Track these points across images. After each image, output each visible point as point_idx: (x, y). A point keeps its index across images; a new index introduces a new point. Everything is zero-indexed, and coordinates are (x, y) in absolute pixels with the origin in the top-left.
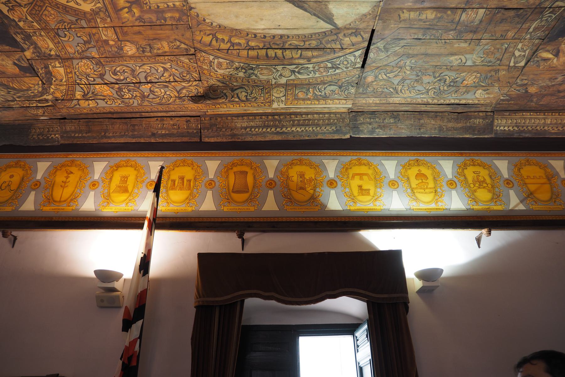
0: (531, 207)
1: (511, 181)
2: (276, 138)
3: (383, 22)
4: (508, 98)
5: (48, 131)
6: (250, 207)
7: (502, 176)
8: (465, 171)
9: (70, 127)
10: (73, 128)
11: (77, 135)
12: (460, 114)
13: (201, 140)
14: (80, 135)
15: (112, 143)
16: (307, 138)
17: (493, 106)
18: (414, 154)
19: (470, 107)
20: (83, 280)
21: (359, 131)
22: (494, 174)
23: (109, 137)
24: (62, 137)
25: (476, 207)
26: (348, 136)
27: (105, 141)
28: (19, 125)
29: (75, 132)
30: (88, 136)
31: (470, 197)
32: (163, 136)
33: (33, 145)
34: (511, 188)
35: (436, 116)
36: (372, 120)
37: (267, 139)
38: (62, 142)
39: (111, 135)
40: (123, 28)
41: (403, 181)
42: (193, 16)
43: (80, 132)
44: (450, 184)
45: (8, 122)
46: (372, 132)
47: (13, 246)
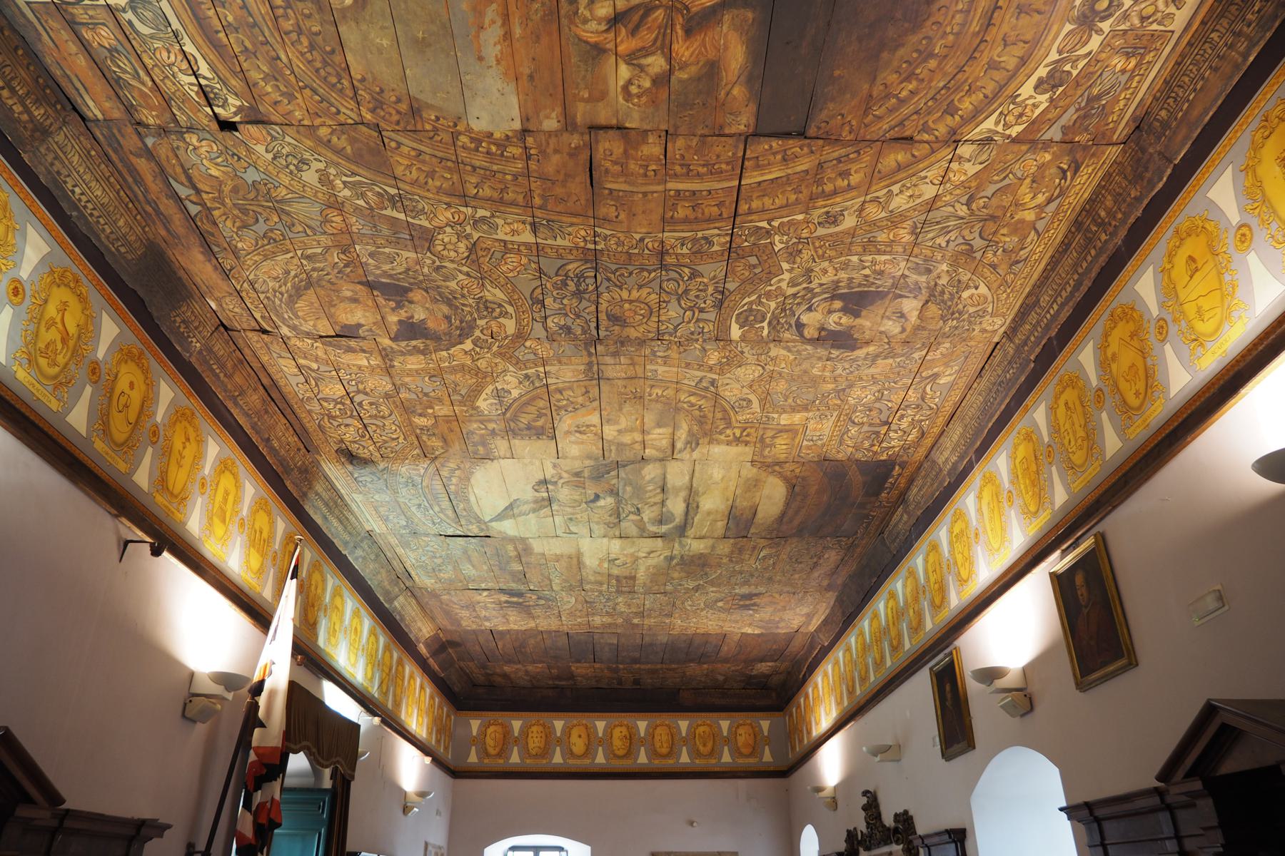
0: (15, 368)
1: (24, 290)
5: (196, 328)
6: (53, 400)
7: (17, 265)
8: (55, 289)
9: (220, 348)
10: (221, 353)
11: (215, 367)
14: (218, 371)
15: (232, 414)
16: (330, 536)
18: (110, 299)
20: (169, 662)
22: (89, 330)
23: (236, 404)
24: (200, 352)
25: (21, 375)
27: (230, 405)
28: (180, 279)
29: (218, 360)
30: (223, 382)
31: (27, 346)
32: (272, 449)
33: (164, 329)
34: (13, 304)
38: (193, 360)
39: (241, 403)
41: (34, 300)
43: (222, 367)
44: (16, 288)
45: (174, 260)
47: (120, 561)
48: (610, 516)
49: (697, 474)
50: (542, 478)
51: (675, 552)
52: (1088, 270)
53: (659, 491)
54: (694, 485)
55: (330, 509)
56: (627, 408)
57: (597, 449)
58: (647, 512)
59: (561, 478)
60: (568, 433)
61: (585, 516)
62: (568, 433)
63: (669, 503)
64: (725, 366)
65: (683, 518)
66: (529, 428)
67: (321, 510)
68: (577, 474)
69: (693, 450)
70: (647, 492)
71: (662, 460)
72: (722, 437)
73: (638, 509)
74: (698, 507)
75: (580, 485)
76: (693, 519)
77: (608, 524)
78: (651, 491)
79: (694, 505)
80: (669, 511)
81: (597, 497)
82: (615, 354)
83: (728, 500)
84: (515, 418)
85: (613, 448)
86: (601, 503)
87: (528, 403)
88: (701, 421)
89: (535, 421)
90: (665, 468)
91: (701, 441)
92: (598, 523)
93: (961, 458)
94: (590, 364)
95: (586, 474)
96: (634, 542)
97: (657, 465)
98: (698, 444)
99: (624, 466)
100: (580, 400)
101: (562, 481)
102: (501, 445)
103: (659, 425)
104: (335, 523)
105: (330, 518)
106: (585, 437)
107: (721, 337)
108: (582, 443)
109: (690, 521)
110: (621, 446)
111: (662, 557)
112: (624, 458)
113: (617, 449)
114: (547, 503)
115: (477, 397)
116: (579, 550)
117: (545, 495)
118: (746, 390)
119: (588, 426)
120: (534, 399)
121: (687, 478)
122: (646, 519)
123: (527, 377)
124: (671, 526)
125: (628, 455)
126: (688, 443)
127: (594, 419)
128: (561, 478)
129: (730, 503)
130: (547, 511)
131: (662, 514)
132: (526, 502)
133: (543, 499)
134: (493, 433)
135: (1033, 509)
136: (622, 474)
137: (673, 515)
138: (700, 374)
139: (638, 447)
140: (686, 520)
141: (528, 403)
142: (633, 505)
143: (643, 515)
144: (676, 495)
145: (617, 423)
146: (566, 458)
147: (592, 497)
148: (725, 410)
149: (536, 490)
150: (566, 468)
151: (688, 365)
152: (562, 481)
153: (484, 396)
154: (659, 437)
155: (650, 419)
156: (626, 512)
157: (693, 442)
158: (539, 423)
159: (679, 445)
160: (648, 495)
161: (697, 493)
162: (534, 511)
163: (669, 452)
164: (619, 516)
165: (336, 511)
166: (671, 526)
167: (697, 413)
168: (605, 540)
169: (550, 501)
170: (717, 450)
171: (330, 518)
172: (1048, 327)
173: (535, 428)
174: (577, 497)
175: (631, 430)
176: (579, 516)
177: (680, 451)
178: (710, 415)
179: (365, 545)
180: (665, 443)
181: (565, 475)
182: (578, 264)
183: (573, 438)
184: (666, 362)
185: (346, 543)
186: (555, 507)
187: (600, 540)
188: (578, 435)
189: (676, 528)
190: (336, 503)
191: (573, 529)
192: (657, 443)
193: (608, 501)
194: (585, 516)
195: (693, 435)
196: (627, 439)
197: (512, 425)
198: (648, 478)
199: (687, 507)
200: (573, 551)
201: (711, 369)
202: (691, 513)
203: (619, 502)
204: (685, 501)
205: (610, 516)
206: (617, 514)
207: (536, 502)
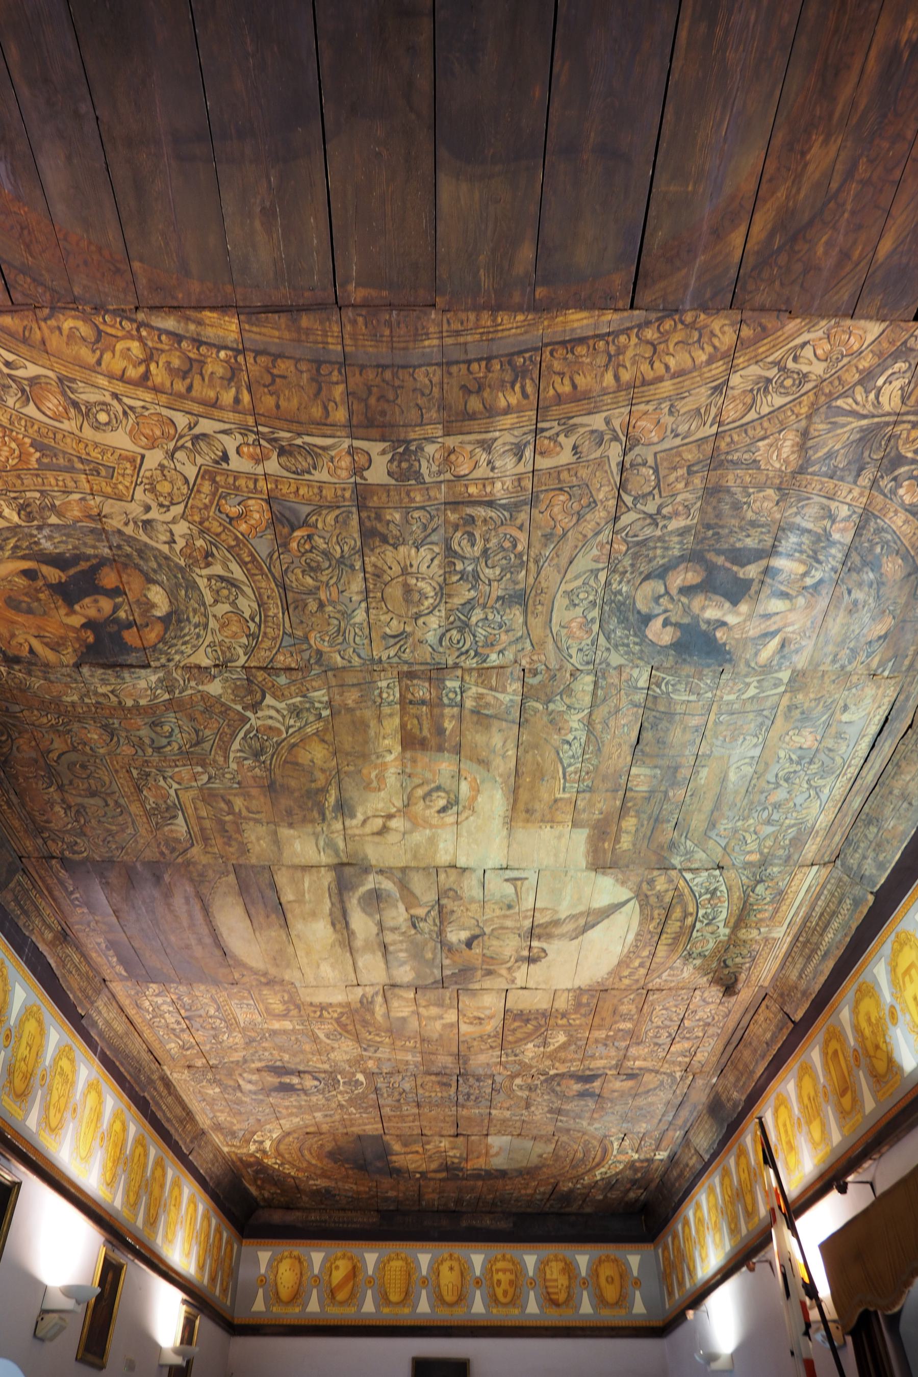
2: (830, 964)
3: (23, 1096)
4: (890, 664)
12: (914, 726)
13: (793, 1022)
16: (848, 939)
17: (653, 1186)
19: (902, 709)
21: (872, 881)
26: (871, 898)
35: (898, 765)
36: (860, 851)
37: (827, 973)
40: (536, 923)
42: (805, 337)
46: (861, 912)
48: (453, 912)
49: (350, 969)
50: (532, 966)
51: (338, 826)
52: (173, 1125)
53: (391, 948)
54: (348, 954)
55: (814, 951)
56: (435, 1036)
57: (464, 1002)
58: (401, 919)
59: (509, 969)
60: (490, 1018)
61: (489, 914)
62: (490, 1018)
63: (374, 930)
64: (358, 1061)
65: (348, 906)
66: (528, 1021)
67: (817, 965)
68: (489, 973)
69: (363, 996)
70: (406, 951)
71: (394, 986)
72: (339, 1010)
73: (414, 926)
74: (333, 924)
75: (489, 959)
76: (332, 904)
77: (458, 897)
78: (401, 950)
79: (338, 926)
80: (370, 915)
81: (469, 944)
82: (445, 1068)
83: (298, 936)
84: (537, 1028)
85: (447, 1001)
86: (464, 935)
87: (521, 1040)
88: (365, 1023)
89: (520, 1027)
90: (390, 976)
91: (359, 1005)
92: (472, 900)
93: (101, 1034)
94: (465, 1063)
95: (479, 973)
96: (415, 857)
97: (398, 981)
98: (361, 1002)
99: (435, 982)
100: (475, 1043)
101: (509, 965)
102: (562, 1004)
103: (404, 1019)
104: (829, 936)
105: (823, 948)
106: (476, 1014)
107: (370, 1075)
108: (479, 1008)
109: (336, 899)
110: (440, 1004)
111: (360, 817)
112: (436, 992)
113: (444, 1000)
114: (536, 931)
115: (564, 1044)
116: (510, 830)
117: (535, 944)
118: (336, 1045)
119: (471, 1023)
120: (516, 1042)
121: (360, 964)
122: (401, 907)
123: (516, 1055)
124: (362, 890)
125: (431, 995)
126: (372, 1002)
127: (464, 1028)
128: (509, 969)
129: (293, 933)
130: (541, 919)
131: (379, 911)
132: (562, 936)
133: (539, 938)
134: (564, 1016)
135: (83, 1154)
136: (437, 972)
137: (364, 910)
138: (378, 1055)
139: (422, 1002)
140: (342, 902)
141: (521, 1040)
142: (421, 932)
143: (405, 915)
144: (366, 941)
145: (445, 1026)
146: (499, 991)
147: (475, 943)
148: (347, 1032)
149: (544, 951)
150: (500, 979)
151: (389, 1060)
152: (509, 965)
153: (557, 1045)
154: (402, 1008)
155: (414, 1024)
156: (430, 921)
157: (366, 1004)
158: (517, 1024)
159: (379, 999)
160: (404, 946)
161: (342, 944)
162: (556, 923)
163: (388, 994)
164: (441, 908)
165: (814, 939)
166: (362, 890)
167: (371, 1029)
168: (462, 862)
169: (532, 934)
170: (338, 997)
171: (823, 948)
172: (157, 1104)
173: (522, 1021)
174: (495, 943)
175: (430, 1018)
176: (498, 912)
177: (377, 993)
178: (358, 1027)
179: (853, 862)
180: (395, 1004)
181: (504, 972)
182: (528, 381)
183: (488, 1012)
184: (407, 1063)
185: (857, 903)
186: (527, 923)
187: (472, 864)
188: (482, 1016)
189: (353, 888)
190: (805, 944)
191: (509, 889)
192: (403, 1003)
193: (457, 936)
194: (489, 914)
195: (368, 1010)
196: (434, 1011)
197: (542, 1022)
198: (407, 968)
199: (347, 924)
200: (521, 834)
201: (370, 1058)
202: (338, 913)
203: (441, 933)
204: (353, 933)
205: (453, 912)
206: (443, 915)
207: (549, 937)
